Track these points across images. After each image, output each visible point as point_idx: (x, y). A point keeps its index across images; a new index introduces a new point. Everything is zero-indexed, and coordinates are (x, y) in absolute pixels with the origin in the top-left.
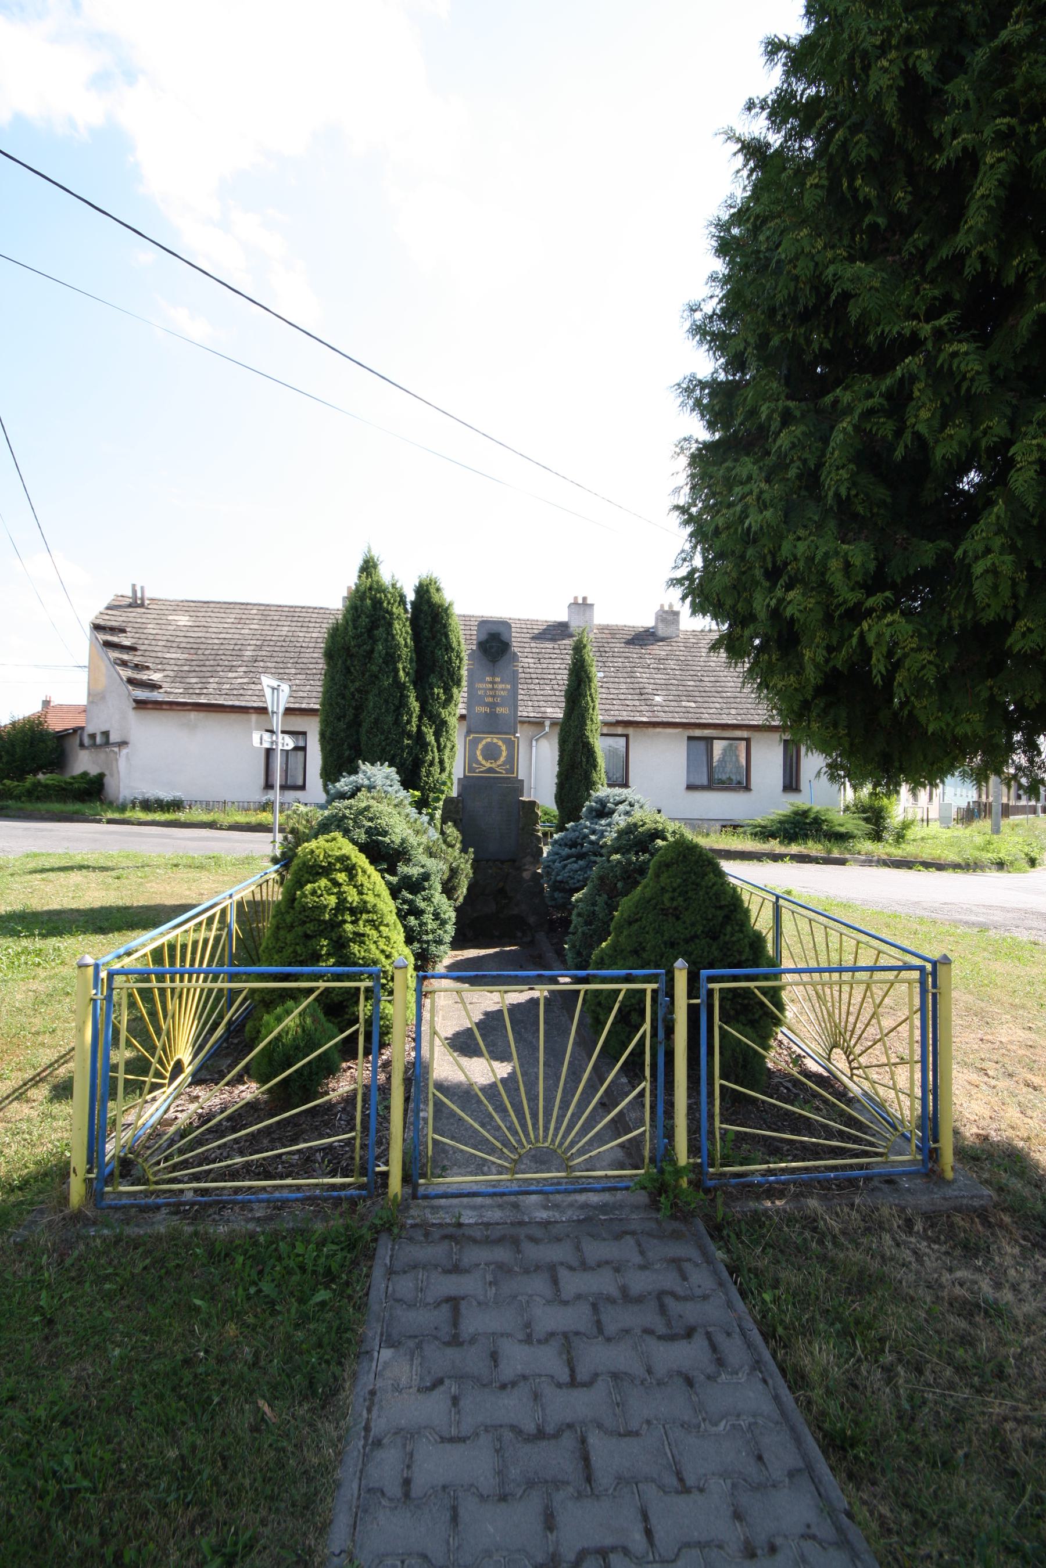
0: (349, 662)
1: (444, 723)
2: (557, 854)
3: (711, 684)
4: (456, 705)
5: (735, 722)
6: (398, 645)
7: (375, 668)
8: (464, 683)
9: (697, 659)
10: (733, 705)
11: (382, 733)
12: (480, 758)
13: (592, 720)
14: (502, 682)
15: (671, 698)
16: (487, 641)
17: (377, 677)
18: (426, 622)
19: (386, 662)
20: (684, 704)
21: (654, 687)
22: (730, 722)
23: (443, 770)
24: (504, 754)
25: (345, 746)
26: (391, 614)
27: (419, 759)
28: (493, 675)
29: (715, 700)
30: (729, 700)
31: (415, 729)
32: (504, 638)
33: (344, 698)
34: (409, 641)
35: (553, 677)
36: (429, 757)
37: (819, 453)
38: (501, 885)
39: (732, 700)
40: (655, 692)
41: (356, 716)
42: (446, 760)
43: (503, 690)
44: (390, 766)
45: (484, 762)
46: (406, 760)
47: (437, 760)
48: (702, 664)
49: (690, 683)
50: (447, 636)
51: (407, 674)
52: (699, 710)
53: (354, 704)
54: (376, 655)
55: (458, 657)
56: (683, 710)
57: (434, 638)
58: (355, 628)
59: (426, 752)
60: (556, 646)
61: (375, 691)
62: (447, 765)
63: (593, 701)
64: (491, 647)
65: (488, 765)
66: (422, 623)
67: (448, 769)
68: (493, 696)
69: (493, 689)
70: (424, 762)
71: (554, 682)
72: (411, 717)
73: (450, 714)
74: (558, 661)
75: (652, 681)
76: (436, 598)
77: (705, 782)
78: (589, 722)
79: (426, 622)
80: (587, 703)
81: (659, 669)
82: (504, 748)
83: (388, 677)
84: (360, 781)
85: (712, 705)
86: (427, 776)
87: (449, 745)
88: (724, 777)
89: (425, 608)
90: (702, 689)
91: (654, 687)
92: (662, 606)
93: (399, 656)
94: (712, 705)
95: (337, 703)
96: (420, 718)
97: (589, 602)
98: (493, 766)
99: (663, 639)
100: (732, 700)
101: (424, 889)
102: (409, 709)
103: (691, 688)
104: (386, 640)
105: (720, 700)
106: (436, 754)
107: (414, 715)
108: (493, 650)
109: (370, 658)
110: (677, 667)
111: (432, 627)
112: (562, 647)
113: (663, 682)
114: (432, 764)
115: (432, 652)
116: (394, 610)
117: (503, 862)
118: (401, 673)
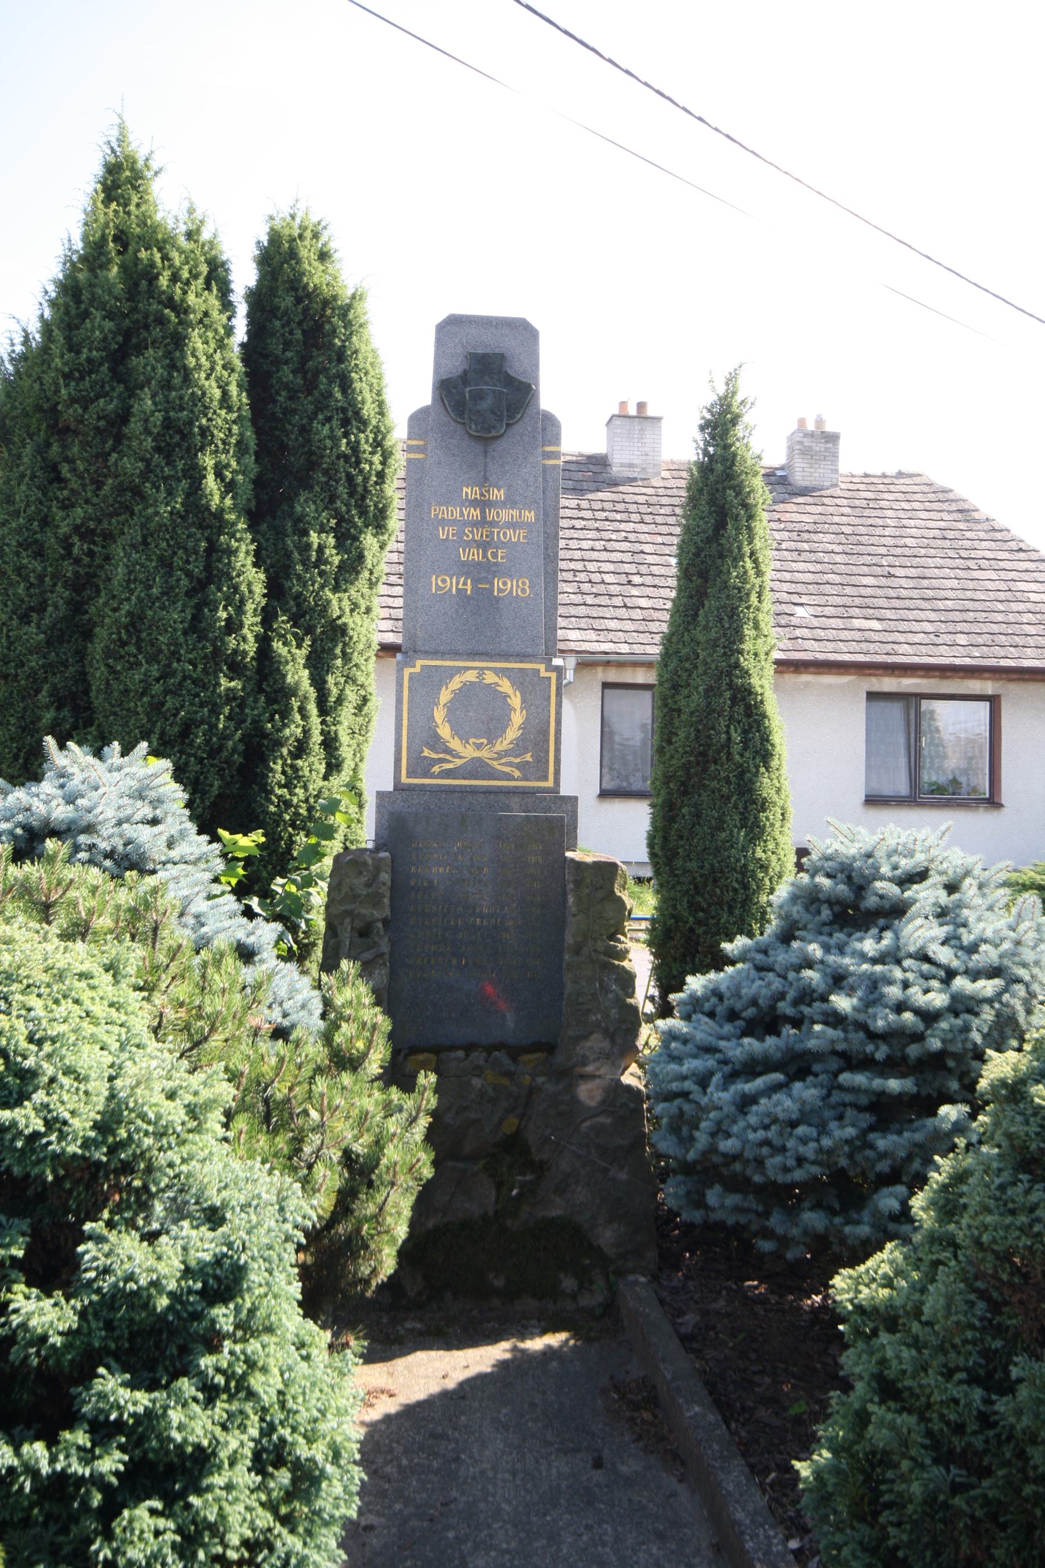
0: (55, 448)
1: (338, 631)
2: (709, 1050)
3: (911, 583)
4: (372, 585)
5: (968, 661)
6: (200, 400)
7: (130, 466)
8: (395, 522)
9: (879, 531)
10: (960, 627)
11: (152, 659)
12: (445, 731)
13: (756, 626)
14: (510, 502)
15: (829, 610)
16: (464, 378)
17: (137, 493)
18: (287, 345)
19: (165, 450)
20: (857, 623)
21: (792, 587)
22: (958, 662)
23: (333, 766)
24: (517, 718)
25: (43, 697)
26: (181, 309)
27: (264, 735)
28: (484, 481)
29: (922, 615)
30: (952, 616)
31: (251, 647)
32: (515, 369)
33: (40, 553)
34: (233, 389)
35: (579, 566)
36: (293, 731)
37: (119, 977)
38: (511, 1124)
39: (958, 616)
40: (796, 599)
41: (77, 607)
42: (344, 738)
43: (512, 525)
44: (156, 753)
45: (455, 744)
46: (224, 737)
47: (317, 738)
48: (889, 541)
49: (866, 581)
50: (346, 385)
51: (229, 487)
52: (890, 637)
53: (68, 569)
54: (135, 426)
55: (378, 444)
56: (857, 635)
57: (310, 386)
58: (74, 348)
59: (285, 714)
60: (584, 504)
61: (133, 533)
62: (346, 752)
63: (759, 574)
64: (477, 396)
65: (469, 752)
66: (275, 346)
67: (348, 765)
68: (484, 545)
69: (483, 522)
70: (279, 743)
71: (582, 577)
72: (240, 610)
73: (355, 606)
74: (591, 534)
75: (788, 576)
76: (316, 276)
77: (903, 788)
78: (748, 631)
79: (287, 345)
80: (744, 577)
81: (800, 552)
82: (516, 701)
83: (170, 493)
84: (40, 808)
85: (916, 627)
86: (288, 785)
87: (352, 696)
88: (942, 779)
89: (286, 301)
90: (892, 593)
91: (792, 587)
92: (802, 422)
93: (204, 431)
94: (916, 627)
95: (19, 570)
96: (268, 617)
97: (650, 412)
98: (484, 754)
99: (804, 492)
100: (958, 616)
101: (212, 1342)
102: (236, 588)
103: (869, 591)
104: (167, 385)
105: (933, 616)
106: (315, 720)
107: (250, 607)
108: (485, 405)
109: (119, 438)
110: (838, 549)
111: (304, 359)
112: (597, 506)
113: (810, 577)
114: (301, 749)
115: (304, 430)
116: (191, 299)
117: (515, 1052)
118: (211, 483)
